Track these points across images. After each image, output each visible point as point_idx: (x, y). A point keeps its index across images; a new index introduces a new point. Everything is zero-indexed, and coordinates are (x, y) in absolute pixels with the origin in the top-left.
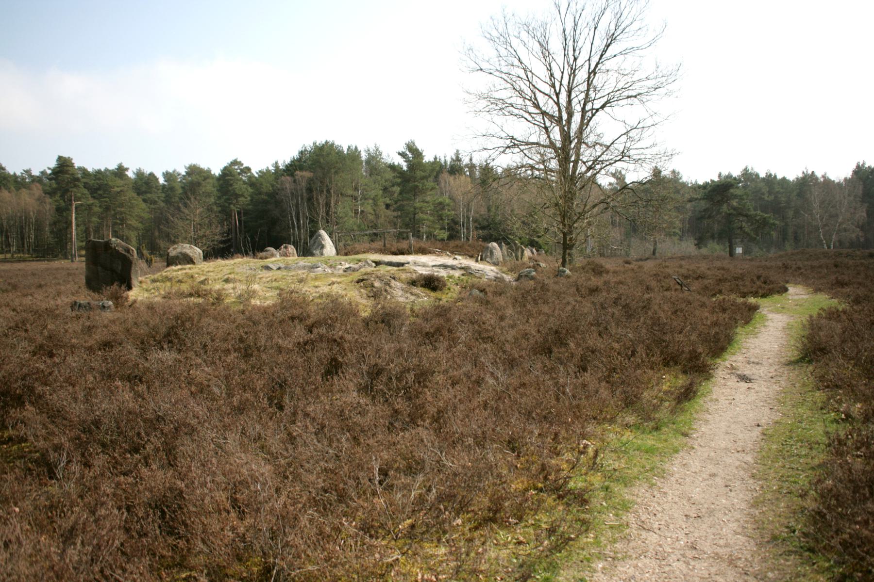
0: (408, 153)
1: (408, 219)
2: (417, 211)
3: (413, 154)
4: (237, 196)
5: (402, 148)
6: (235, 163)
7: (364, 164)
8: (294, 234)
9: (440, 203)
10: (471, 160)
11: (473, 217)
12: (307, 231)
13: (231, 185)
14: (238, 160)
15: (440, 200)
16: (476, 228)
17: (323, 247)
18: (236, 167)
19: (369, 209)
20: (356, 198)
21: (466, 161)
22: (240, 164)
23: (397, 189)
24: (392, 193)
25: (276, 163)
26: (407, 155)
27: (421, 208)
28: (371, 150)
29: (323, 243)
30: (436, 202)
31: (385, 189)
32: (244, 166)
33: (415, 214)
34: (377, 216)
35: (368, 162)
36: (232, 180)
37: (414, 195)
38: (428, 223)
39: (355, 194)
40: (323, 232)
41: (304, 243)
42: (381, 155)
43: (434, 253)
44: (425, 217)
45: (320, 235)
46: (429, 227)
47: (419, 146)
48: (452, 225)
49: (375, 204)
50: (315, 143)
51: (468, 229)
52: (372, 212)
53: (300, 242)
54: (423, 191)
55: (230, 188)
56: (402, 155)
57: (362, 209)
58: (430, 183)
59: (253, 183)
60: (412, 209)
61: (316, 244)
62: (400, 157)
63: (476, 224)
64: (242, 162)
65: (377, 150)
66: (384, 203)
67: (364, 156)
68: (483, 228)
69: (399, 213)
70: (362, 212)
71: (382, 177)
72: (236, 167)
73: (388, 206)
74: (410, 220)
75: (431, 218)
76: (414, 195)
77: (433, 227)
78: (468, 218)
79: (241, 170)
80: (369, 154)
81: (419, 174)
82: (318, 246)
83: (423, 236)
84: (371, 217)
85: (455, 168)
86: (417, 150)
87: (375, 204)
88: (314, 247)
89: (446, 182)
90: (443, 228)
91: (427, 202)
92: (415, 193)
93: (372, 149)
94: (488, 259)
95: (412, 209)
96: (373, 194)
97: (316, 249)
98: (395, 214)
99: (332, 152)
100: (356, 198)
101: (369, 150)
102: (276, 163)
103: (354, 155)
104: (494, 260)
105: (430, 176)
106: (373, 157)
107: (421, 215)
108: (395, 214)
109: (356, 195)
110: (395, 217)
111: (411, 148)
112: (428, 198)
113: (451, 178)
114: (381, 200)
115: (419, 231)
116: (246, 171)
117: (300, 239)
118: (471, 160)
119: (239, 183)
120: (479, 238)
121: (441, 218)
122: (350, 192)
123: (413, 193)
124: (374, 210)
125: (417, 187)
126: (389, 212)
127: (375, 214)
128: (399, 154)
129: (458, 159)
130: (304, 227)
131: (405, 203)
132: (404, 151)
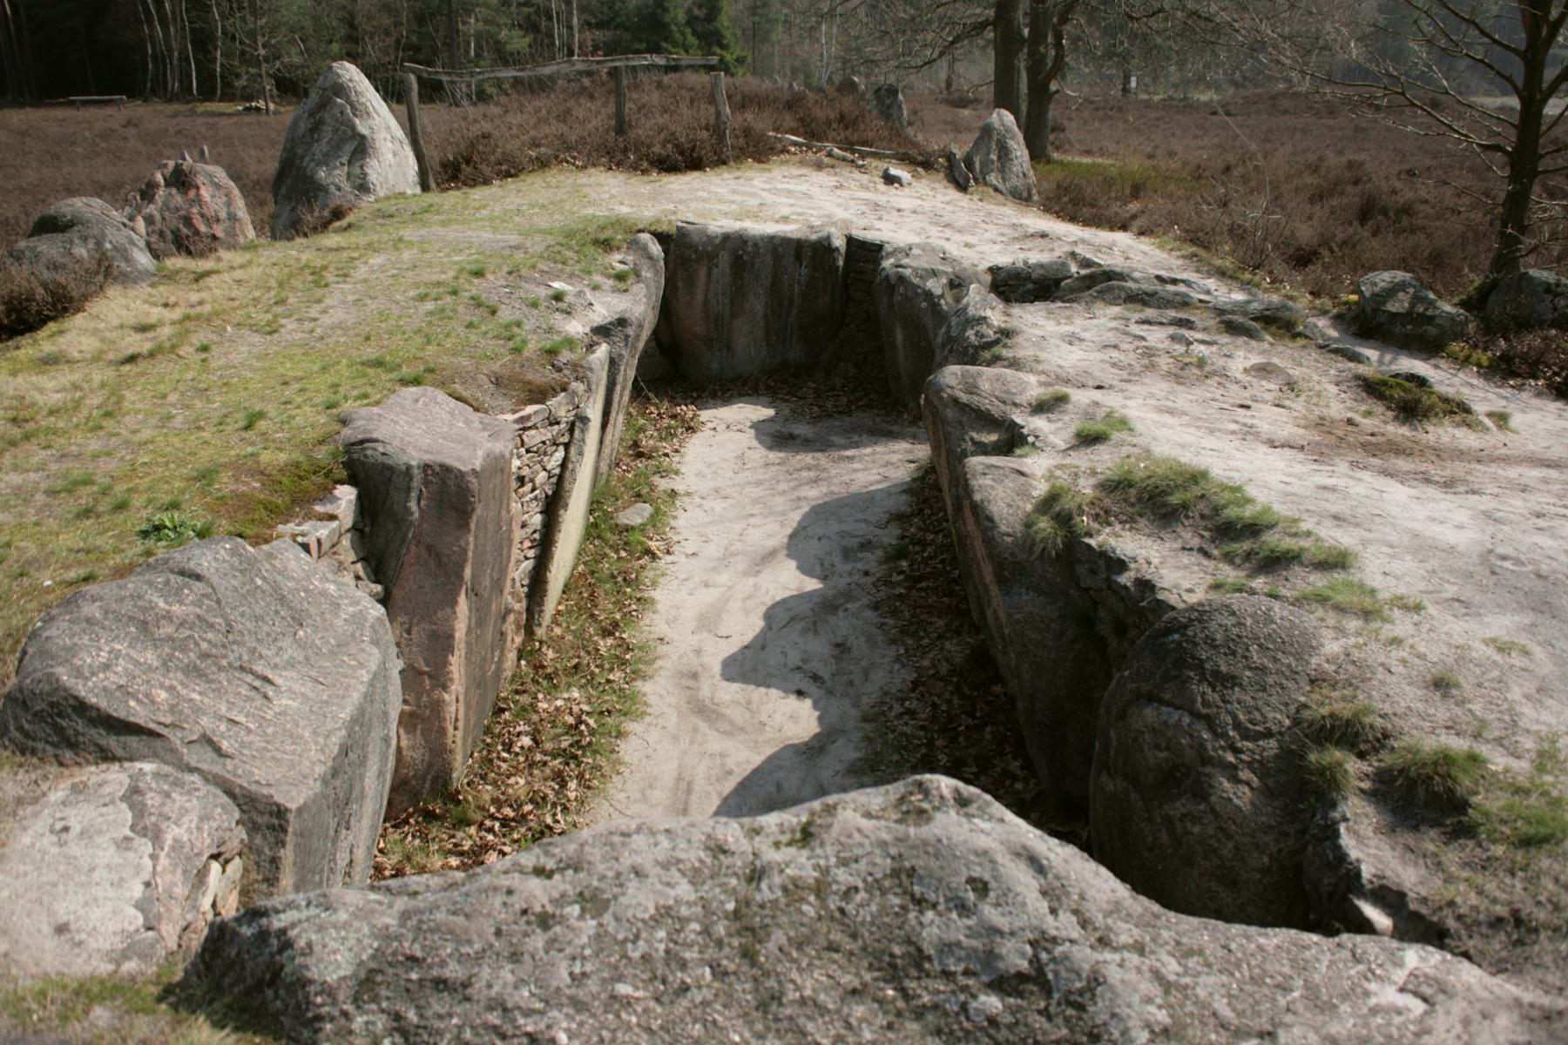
8: (152, 37)
12: (183, 29)
17: (361, 148)
29: (362, 129)
41: (180, 59)
43: (785, 151)
45: (340, 90)
46: (486, 22)
51: (570, 27)
53: (171, 58)
61: (327, 133)
63: (585, 16)
68: (600, 25)
82: (337, 147)
88: (319, 149)
94: (993, 178)
97: (326, 160)
104: (1015, 181)
117: (170, 50)
130: (175, 19)
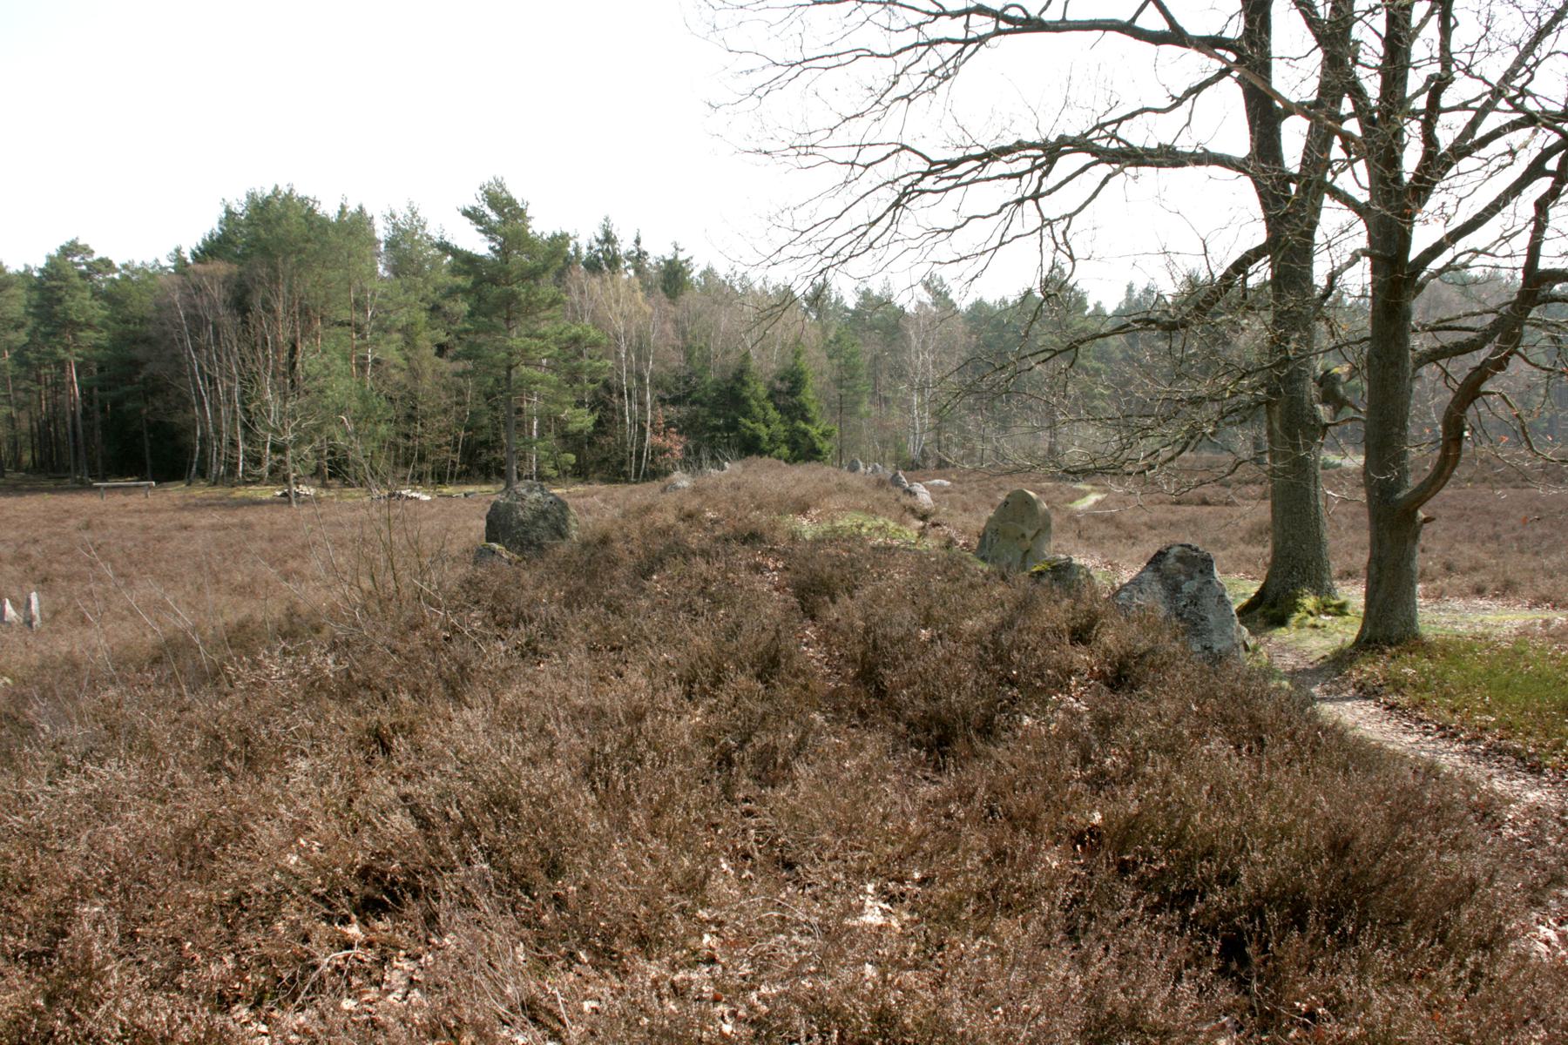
0: (488, 211)
1: (491, 381)
2: (516, 359)
3: (500, 212)
4: (75, 326)
5: (473, 199)
6: (70, 249)
7: (382, 246)
9: (576, 340)
10: (638, 242)
11: (652, 374)
13: (60, 301)
14: (81, 243)
15: (575, 330)
16: (663, 401)
18: (76, 259)
19: (391, 352)
20: (359, 329)
21: (625, 246)
22: (87, 251)
23: (463, 307)
24: (449, 318)
25: (178, 251)
26: (484, 215)
27: (526, 350)
28: (400, 216)
30: (564, 336)
31: (435, 309)
32: (96, 257)
33: (510, 368)
34: (415, 375)
35: (392, 244)
36: (60, 288)
37: (508, 320)
38: (544, 389)
39: (356, 316)
40: (1407, 178)
42: (423, 227)
44: (537, 374)
47: (517, 193)
48: (603, 394)
49: (410, 343)
50: (252, 197)
51: (642, 404)
52: (401, 361)
54: (530, 308)
55: (58, 308)
56: (473, 215)
57: (377, 355)
58: (547, 289)
59: (113, 298)
60: (503, 355)
62: (467, 220)
63: (659, 392)
64: (92, 247)
65: (414, 214)
66: (432, 341)
67: (382, 231)
68: (675, 401)
69: (470, 365)
70: (377, 362)
71: (426, 281)
72: (76, 259)
73: (441, 349)
74: (497, 380)
75: (553, 378)
76: (508, 320)
77: (555, 401)
78: (641, 378)
79: (89, 265)
80: (395, 226)
81: (520, 259)
83: (530, 424)
84: (397, 376)
85: (604, 261)
86: (511, 202)
87: (410, 343)
89: (582, 292)
90: (580, 404)
91: (542, 337)
92: (509, 313)
93: (402, 214)
95: (503, 355)
96: (402, 319)
98: (460, 366)
99: (291, 214)
100: (359, 329)
101: (393, 216)
102: (178, 251)
103: (355, 226)
105: (546, 269)
106: (405, 232)
107: (524, 370)
108: (460, 366)
109: (362, 321)
110: (457, 374)
111: (499, 200)
112: (544, 328)
113: (595, 282)
114: (424, 334)
115: (520, 411)
116: (103, 268)
118: (638, 242)
119: (79, 295)
120: (669, 424)
121: (574, 377)
122: (345, 315)
123: (504, 313)
124: (407, 359)
125: (513, 296)
126: (445, 365)
127: (412, 369)
128: (466, 213)
129: (608, 238)
131: (481, 339)
132: (476, 204)
